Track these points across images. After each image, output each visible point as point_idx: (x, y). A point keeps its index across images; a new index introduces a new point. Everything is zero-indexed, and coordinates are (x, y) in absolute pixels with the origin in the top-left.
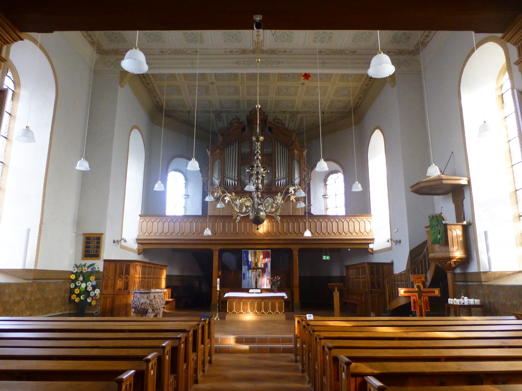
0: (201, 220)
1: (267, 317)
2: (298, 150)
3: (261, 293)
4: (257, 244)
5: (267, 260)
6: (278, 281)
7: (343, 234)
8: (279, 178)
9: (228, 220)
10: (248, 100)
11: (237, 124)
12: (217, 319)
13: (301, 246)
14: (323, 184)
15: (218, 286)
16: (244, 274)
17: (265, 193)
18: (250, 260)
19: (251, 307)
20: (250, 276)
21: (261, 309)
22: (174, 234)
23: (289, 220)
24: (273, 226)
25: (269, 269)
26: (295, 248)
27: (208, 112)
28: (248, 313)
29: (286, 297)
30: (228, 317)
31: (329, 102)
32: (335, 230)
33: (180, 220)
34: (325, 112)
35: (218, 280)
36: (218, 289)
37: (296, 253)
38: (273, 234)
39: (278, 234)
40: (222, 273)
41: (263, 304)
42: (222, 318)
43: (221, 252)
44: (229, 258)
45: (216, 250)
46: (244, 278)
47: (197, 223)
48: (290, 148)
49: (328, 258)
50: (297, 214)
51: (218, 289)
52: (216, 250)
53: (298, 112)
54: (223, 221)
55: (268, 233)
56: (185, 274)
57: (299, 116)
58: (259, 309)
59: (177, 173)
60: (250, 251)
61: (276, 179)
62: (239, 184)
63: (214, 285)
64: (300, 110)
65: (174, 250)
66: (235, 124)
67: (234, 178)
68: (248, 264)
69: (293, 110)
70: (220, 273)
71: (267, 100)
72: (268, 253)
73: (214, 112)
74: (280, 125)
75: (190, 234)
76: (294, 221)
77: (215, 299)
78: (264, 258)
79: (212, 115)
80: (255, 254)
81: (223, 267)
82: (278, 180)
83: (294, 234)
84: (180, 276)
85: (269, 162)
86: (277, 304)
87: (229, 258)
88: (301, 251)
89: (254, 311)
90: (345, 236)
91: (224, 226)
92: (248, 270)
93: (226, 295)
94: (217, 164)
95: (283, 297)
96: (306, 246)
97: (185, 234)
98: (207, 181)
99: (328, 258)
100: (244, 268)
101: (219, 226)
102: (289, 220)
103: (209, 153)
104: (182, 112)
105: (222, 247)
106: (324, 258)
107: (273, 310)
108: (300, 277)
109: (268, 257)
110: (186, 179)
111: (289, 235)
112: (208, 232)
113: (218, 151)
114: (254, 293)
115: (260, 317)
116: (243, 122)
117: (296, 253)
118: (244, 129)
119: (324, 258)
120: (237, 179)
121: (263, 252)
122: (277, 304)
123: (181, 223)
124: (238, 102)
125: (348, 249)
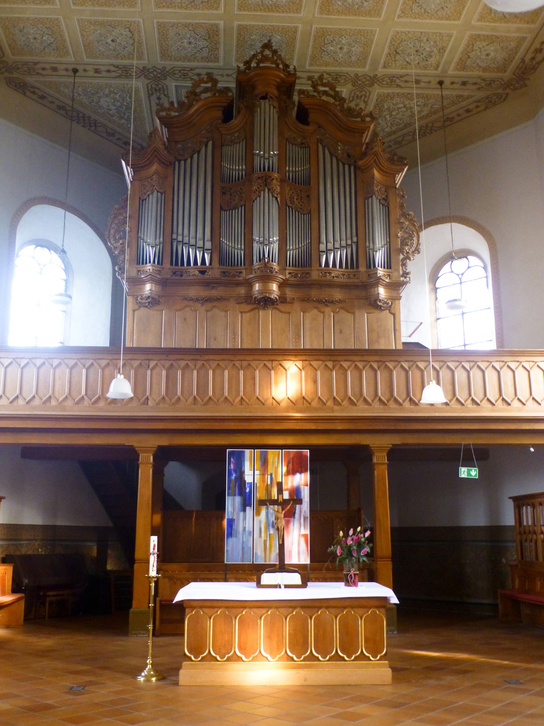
0: (104, 363)
1: (327, 673)
2: (380, 170)
3: (304, 585)
4: (265, 430)
5: (301, 480)
6: (360, 546)
7: (516, 404)
8: (330, 246)
9: (183, 363)
10: (241, 28)
11: (208, 95)
12: (148, 680)
13: (396, 440)
14: (427, 287)
15: (153, 560)
16: (231, 522)
17: (292, 286)
18: (248, 479)
19: (268, 637)
20: (249, 527)
21: (305, 645)
22: (21, 402)
23: (360, 365)
24: (315, 382)
25: (305, 507)
26: (380, 444)
27: (125, 72)
28: (260, 657)
29: (394, 600)
30: (187, 675)
31: (466, 38)
32: (492, 394)
33: (38, 362)
34: (447, 82)
35: (154, 540)
36: (153, 572)
37: (380, 460)
38: (314, 404)
39: (330, 403)
40: (164, 519)
41: (311, 624)
42: (168, 673)
43: (163, 456)
44: (183, 480)
45: (146, 447)
46: (230, 535)
47: (92, 370)
48: (360, 163)
49: (474, 473)
50: (382, 347)
51: (153, 572)
52: (146, 447)
53: (374, 80)
54: (168, 364)
55: (301, 402)
56: (60, 522)
57: (377, 91)
58: (299, 644)
59: (43, 252)
60: (247, 452)
61: (323, 247)
62: (216, 264)
63: (138, 554)
64: (381, 71)
65: (29, 452)
66: (204, 96)
67: (200, 244)
68: (242, 492)
69: (360, 70)
70: (158, 518)
71: (296, 28)
72: (300, 458)
73: (144, 72)
74: (332, 101)
75: (69, 403)
76: (375, 365)
77: (142, 601)
78: (292, 472)
79: (138, 84)
80: (265, 462)
81: (164, 501)
82: (327, 251)
83: (376, 404)
84: (44, 528)
85: (301, 202)
86: (361, 624)
87: (183, 480)
88: (395, 454)
89: (279, 649)
90: (519, 410)
91: (171, 381)
92: (244, 510)
93: (183, 595)
94: (152, 204)
95: (386, 599)
96: (411, 440)
97: (53, 403)
98: (123, 252)
99: (474, 473)
100: (232, 503)
101: (158, 378)
102: (360, 365)
103: (128, 172)
104: (55, 69)
105: (164, 441)
106: (464, 472)
107: (349, 646)
108: (391, 528)
109: (302, 471)
110: (68, 269)
111: (361, 405)
112: (121, 387)
113: (155, 167)
114: (281, 587)
115: (303, 673)
116: (228, 89)
117: (380, 460)
118: (227, 116)
119: (464, 472)
120: (208, 245)
121: (287, 454)
122: (361, 624)
123: (42, 370)
124: (212, 33)
125: (527, 446)
